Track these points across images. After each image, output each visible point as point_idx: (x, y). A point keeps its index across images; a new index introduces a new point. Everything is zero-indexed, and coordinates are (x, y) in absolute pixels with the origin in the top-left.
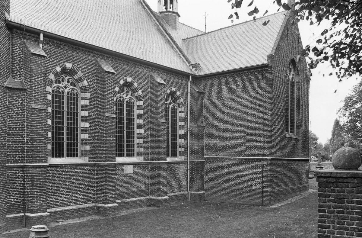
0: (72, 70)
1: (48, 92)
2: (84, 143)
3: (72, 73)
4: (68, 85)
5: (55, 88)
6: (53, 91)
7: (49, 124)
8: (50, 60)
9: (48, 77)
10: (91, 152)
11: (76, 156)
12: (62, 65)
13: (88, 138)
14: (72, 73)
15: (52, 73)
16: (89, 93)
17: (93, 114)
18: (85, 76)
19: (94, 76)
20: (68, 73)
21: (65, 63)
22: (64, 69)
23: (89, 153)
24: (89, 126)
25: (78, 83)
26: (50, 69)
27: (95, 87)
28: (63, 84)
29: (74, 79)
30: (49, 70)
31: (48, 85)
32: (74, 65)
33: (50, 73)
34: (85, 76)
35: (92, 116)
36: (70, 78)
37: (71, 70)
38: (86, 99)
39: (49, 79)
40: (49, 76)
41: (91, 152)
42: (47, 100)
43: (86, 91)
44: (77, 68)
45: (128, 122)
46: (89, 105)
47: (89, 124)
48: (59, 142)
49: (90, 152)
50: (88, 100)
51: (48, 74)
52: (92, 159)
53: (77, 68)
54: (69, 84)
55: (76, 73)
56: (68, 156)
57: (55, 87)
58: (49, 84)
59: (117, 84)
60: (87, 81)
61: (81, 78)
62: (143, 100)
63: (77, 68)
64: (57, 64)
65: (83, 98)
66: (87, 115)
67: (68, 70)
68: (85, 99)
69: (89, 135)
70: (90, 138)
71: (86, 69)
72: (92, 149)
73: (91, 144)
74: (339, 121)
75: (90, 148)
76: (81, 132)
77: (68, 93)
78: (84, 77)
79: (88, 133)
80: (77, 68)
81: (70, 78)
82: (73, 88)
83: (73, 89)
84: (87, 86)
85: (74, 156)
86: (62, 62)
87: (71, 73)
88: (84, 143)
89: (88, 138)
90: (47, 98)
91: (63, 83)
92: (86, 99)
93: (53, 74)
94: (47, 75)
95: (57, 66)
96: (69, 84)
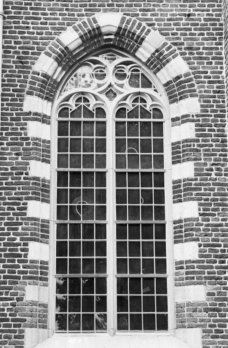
0: (123, 34)
1: (29, 113)
2: (185, 276)
3: (128, 45)
4: (122, 86)
5: (129, 102)
6: (63, 112)
7: (31, 216)
8: (40, 16)
9: (30, 68)
10: (212, 310)
11: (159, 328)
12: (84, 23)
13: (195, 256)
14: (128, 45)
15: (47, 54)
16: (197, 99)
17: (218, 169)
18: (175, 44)
19: (215, 39)
20: (113, 46)
21: (95, 16)
22: (96, 36)
23: (205, 315)
24: (200, 215)
25: (155, 74)
26: (37, 44)
27: (221, 73)
28: (99, 86)
29: (140, 60)
30: (36, 46)
31: (30, 93)
32: (128, 15)
33: (39, 54)
34: (175, 44)
35: (213, 176)
36: (127, 63)
37: (120, 32)
38: (185, 119)
39: (34, 73)
40: (33, 64)
41: (212, 310)
42: (28, 139)
43: (183, 93)
44: (140, 25)
45: (182, 183)
46: (198, 141)
47: (200, 205)
48: (98, 279)
49: (206, 310)
50: (193, 121)
51: (31, 58)
52: (217, 337)
53: (144, 24)
54: (126, 81)
55: (140, 40)
56: (121, 326)
57: (71, 95)
58: (35, 89)
60: (185, 59)
61: (161, 54)
63: (140, 25)
64: (64, 24)
65: (177, 119)
66: (191, 174)
67: (112, 37)
68: (183, 122)
69: (200, 246)
70: (207, 256)
71: (177, 19)
72: (216, 299)
73: (213, 279)
74: (99, 57)
75: (209, 294)
76: (175, 237)
77: (120, 112)
78: (174, 47)
79: (198, 240)
80: (144, 24)
81: (127, 63)
82: (139, 93)
83: (139, 98)
84: (187, 75)
85: (149, 327)
86: (83, 15)
87: (124, 43)
88: (185, 276)
89: (195, 256)
90: (26, 134)
91: (101, 82)
92: (185, 119)
93: (50, 55)
94: (27, 63)
95: (64, 29)
96: (126, 81)
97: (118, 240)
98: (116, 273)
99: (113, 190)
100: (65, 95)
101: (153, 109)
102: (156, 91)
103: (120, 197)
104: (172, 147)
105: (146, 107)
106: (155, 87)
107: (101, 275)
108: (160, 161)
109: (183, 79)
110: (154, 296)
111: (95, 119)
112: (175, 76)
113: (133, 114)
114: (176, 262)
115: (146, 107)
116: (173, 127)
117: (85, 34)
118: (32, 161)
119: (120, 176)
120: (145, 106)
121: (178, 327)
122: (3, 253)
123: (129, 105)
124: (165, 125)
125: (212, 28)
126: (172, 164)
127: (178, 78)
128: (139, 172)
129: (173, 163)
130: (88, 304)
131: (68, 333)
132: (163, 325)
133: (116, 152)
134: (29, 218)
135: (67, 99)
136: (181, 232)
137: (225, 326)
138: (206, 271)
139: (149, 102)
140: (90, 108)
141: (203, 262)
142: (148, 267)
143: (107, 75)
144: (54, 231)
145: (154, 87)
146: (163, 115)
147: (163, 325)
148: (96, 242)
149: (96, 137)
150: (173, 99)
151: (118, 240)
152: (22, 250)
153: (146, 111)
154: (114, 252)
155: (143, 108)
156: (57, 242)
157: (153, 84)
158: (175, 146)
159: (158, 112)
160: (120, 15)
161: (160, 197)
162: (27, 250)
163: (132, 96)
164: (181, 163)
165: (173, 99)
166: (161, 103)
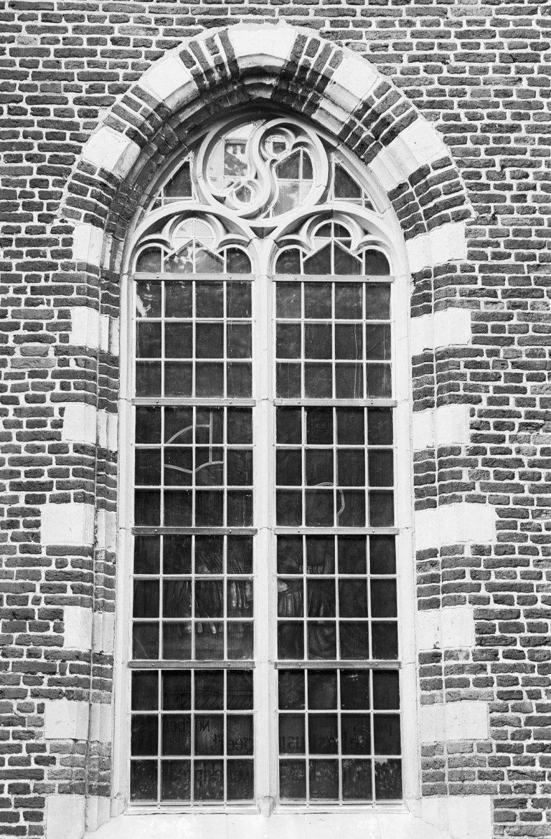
59: (104, 103)
62: (459, 217)
77: (287, 260)
97: (286, 757)
98: (275, 659)
99: (270, 625)
100: (152, 217)
101: (368, 252)
102: (369, 206)
103: (286, 467)
104: (416, 478)
105: (349, 247)
106: (368, 195)
107: (239, 402)
108: (383, 507)
109: (434, 174)
110: (367, 622)
111: (363, 277)
112: (413, 169)
113: (319, 262)
114: (415, 454)
115: (349, 247)
116: (409, 241)
117: (209, 72)
118: (77, 308)
119: (286, 418)
120: (348, 244)
121: (428, 792)
122: (6, 507)
123: (311, 243)
124: (396, 413)
125: (519, 547)
126: (414, 410)
127: (422, 172)
128: (334, 535)
129: (414, 313)
130: (209, 600)
131: (159, 806)
132: (390, 787)
133: (277, 357)
134: (74, 348)
135: (158, 226)
136: (427, 286)
137: (544, 628)
138: (490, 324)
139: (357, 238)
140: (352, 251)
141: (480, 353)
142: (354, 640)
143: (259, 531)
144: (127, 472)
145: (366, 197)
146: (390, 265)
147: (390, 787)
148: (229, 761)
149: (230, 445)
150: (412, 228)
151: (286, 757)
152: (53, 327)
153: (350, 258)
154: (272, 479)
155: (344, 252)
156: (138, 451)
157: (363, 190)
158: (422, 365)
159: (378, 262)
160: (291, 33)
161: (386, 598)
162: (68, 327)
163: (317, 218)
164: (438, 607)
165: (412, 228)
166: (386, 237)
